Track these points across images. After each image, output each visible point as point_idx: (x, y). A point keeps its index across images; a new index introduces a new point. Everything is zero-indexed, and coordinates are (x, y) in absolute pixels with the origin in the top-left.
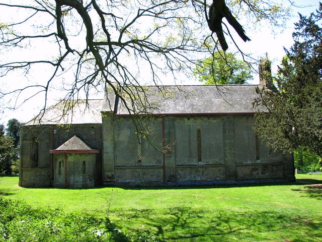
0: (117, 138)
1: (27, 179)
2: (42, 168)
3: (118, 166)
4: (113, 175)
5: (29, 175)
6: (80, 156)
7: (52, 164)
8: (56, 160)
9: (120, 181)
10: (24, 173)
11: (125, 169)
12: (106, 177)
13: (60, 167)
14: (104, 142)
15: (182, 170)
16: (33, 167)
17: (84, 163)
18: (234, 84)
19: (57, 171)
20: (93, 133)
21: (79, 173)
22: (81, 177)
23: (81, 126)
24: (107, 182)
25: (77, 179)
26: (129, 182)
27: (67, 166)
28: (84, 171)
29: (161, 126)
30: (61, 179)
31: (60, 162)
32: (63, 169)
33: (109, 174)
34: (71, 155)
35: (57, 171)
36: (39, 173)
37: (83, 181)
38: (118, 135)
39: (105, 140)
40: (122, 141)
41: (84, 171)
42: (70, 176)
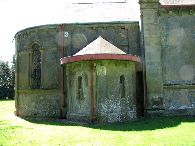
0: (166, 41)
1: (25, 106)
2: (46, 89)
3: (168, 85)
4: (161, 99)
5: (29, 100)
6: (116, 65)
7: (62, 83)
8: (72, 74)
9: (171, 108)
10: (21, 97)
11: (179, 89)
12: (151, 102)
13: (80, 86)
14: (146, 47)
15: (130, 117)
16: (33, 88)
17: (122, 78)
18: (31, 64)
19: (75, 94)
20: (124, 36)
21: (116, 96)
22: (120, 102)
23: (95, 26)
24: (153, 109)
25: (113, 106)
26: (186, 110)
27: (94, 84)
28: (123, 95)
29: (110, 59)
30: (82, 108)
31: (80, 79)
32: (86, 89)
33: (156, 97)
34: (101, 65)
35: (75, 94)
36: (42, 98)
37: (122, 111)
38: (167, 36)
39: (148, 44)
40: (172, 46)
41: (123, 95)
42: (100, 102)
